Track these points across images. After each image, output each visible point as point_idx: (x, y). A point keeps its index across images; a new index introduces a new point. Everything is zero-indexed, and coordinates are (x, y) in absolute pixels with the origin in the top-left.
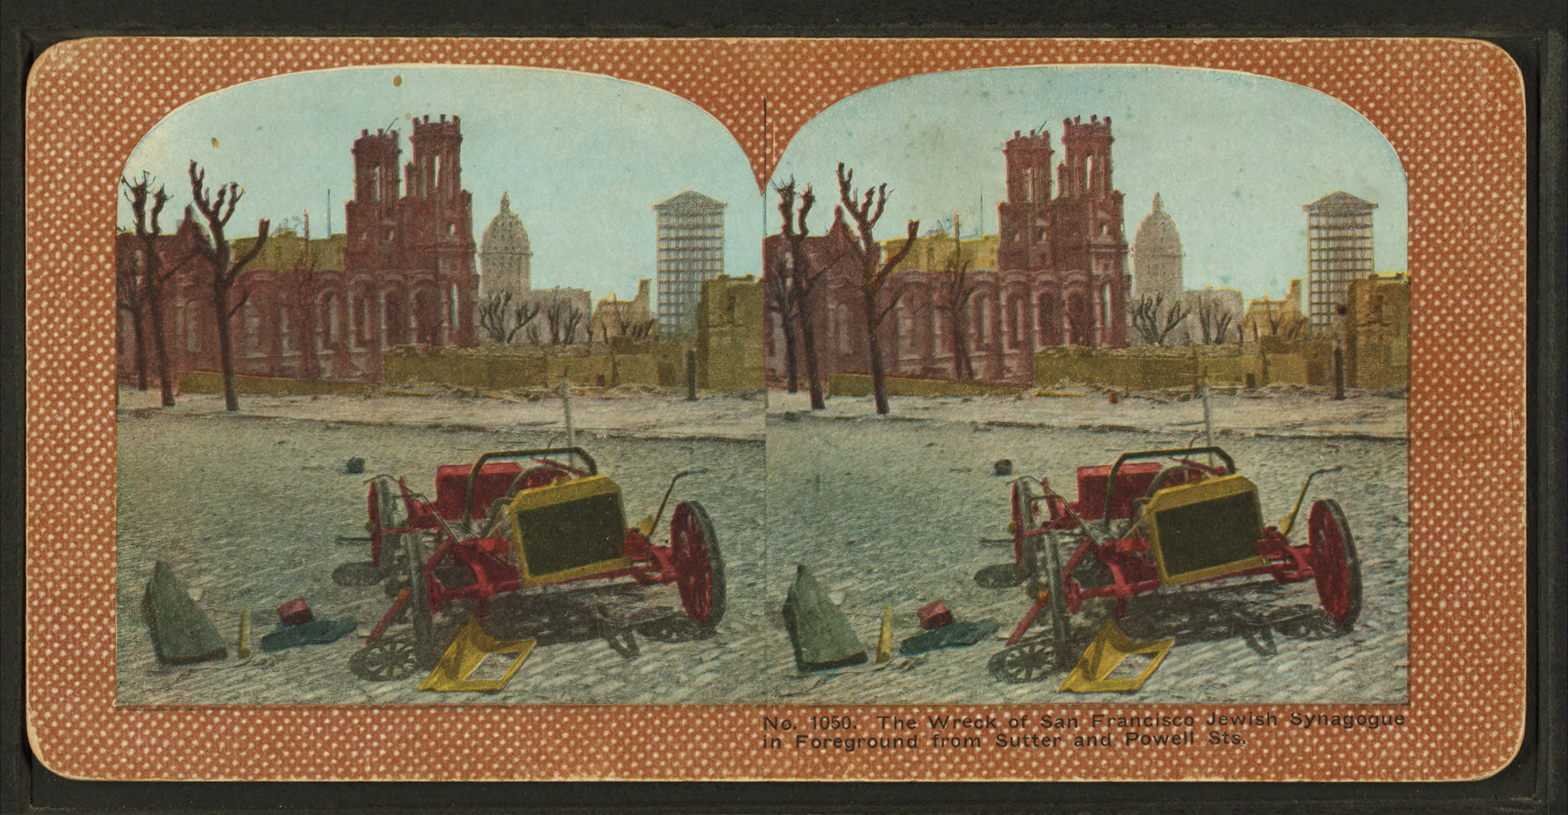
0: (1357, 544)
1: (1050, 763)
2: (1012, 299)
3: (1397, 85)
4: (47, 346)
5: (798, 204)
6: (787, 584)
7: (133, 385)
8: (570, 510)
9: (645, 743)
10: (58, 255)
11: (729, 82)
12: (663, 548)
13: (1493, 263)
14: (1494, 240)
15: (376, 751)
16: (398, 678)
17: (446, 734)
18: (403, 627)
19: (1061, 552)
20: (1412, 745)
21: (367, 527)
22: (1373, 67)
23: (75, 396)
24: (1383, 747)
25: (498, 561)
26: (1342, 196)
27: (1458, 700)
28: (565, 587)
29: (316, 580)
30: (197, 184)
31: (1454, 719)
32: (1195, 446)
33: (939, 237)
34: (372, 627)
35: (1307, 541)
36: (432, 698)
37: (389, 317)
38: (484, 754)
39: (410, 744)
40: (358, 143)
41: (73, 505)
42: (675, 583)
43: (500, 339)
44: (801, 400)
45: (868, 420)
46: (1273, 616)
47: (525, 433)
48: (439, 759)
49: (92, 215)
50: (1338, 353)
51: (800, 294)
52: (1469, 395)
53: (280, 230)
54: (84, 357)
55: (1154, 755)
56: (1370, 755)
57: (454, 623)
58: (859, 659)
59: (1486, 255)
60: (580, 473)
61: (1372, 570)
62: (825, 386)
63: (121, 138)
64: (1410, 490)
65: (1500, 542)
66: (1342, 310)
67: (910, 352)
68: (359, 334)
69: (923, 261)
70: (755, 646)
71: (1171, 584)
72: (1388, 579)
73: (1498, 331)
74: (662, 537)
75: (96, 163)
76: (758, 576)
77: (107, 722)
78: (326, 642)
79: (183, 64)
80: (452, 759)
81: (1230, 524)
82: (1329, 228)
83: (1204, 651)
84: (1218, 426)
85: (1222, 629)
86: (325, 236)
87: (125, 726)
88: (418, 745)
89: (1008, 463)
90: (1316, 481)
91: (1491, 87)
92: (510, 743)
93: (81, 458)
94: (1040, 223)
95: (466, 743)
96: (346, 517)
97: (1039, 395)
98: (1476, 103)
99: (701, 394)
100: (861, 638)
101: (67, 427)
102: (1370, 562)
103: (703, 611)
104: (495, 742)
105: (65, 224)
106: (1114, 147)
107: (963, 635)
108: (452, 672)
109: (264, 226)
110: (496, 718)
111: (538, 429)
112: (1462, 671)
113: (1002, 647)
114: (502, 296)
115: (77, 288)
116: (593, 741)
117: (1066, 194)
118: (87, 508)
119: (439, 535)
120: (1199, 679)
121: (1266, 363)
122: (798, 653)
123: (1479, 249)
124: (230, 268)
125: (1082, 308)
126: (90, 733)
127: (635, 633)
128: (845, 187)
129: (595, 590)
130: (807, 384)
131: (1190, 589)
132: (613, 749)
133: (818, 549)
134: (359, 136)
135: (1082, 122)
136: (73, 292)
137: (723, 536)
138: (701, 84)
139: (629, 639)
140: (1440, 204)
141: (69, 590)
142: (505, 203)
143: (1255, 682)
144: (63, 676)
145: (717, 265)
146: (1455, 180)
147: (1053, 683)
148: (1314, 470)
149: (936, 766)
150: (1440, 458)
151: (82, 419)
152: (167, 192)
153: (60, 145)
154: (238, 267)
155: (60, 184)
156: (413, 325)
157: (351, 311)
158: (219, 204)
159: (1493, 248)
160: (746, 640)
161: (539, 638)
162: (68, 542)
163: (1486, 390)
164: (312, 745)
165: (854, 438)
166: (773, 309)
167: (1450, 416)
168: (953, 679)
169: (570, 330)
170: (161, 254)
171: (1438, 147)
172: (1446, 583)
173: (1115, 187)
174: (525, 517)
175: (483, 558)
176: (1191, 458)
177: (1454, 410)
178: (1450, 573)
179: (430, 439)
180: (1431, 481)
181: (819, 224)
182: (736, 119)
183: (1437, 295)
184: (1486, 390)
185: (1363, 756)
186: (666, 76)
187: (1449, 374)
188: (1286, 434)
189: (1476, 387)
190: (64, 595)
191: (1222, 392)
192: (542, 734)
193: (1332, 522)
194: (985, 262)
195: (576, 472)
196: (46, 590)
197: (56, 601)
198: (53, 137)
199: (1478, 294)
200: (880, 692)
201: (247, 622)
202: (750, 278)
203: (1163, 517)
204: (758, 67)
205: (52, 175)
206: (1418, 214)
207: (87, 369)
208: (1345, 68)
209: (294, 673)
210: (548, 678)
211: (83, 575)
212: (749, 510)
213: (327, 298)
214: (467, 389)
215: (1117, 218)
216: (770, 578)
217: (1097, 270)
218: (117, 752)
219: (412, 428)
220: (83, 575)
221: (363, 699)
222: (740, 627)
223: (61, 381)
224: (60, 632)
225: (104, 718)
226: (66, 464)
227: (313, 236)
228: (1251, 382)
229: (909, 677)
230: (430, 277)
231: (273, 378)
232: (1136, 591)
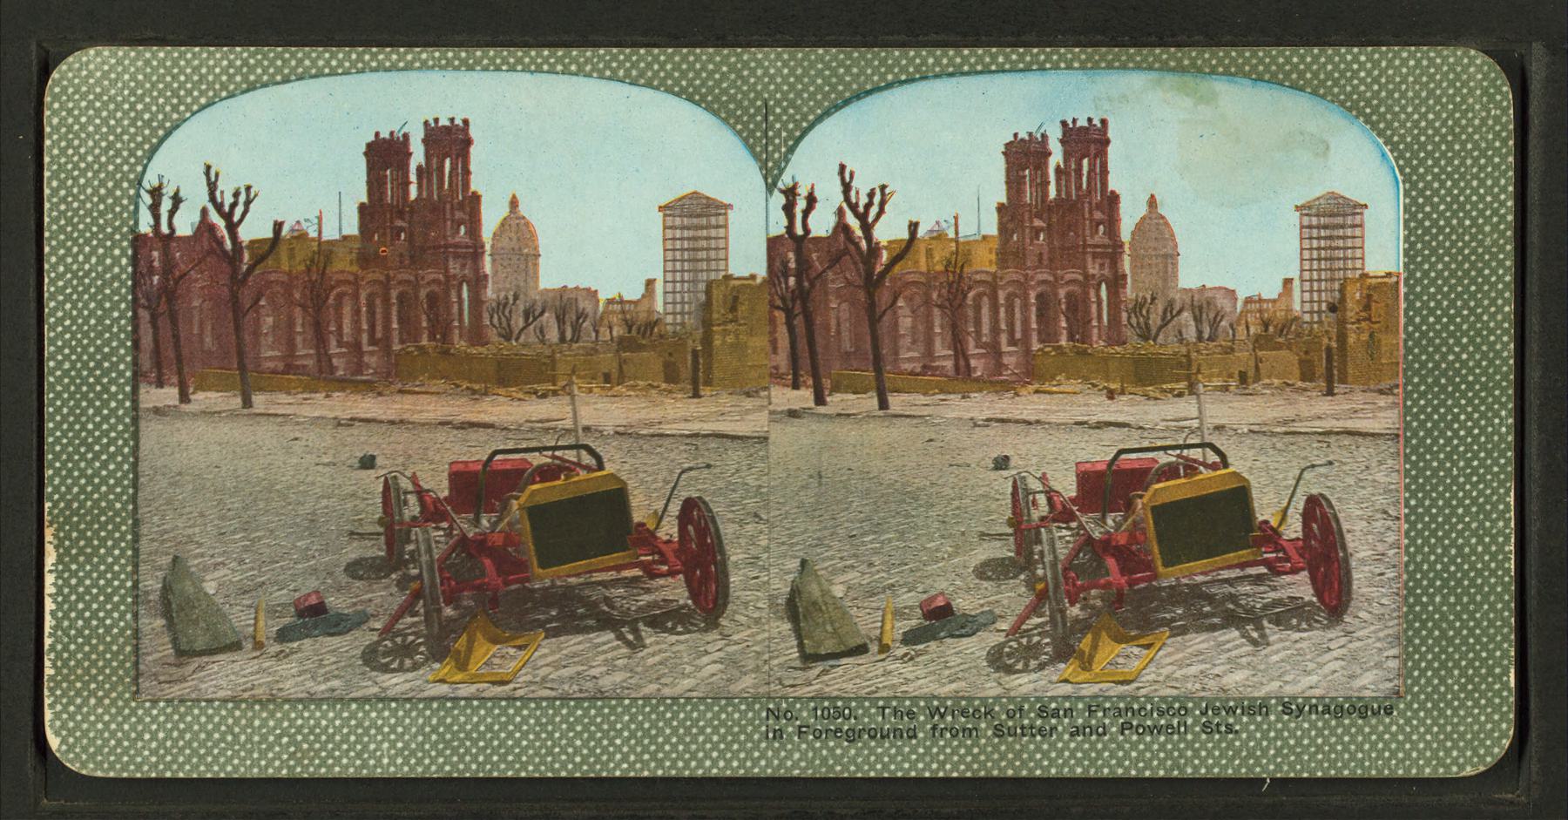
0: (1348, 537)
1: (1053, 755)
2: (1010, 298)
4: (70, 347)
5: (801, 204)
6: (790, 578)
7: (150, 383)
8: (1201, 503)
9: (657, 736)
10: (81, 258)
11: (739, 89)
12: (669, 542)
13: (1487, 264)
14: (1488, 242)
15: (393, 744)
16: (1034, 671)
17: (462, 728)
18: (1040, 620)
19: (1058, 545)
20: (1408, 738)
21: (380, 522)
22: (1369, 73)
23: (99, 396)
24: (1380, 738)
25: (522, 553)
26: (695, 196)
27: (1453, 692)
28: (573, 580)
29: (330, 574)
30: (212, 187)
31: (1449, 712)
32: (1189, 441)
33: (939, 236)
35: (1300, 535)
36: (443, 689)
37: (1040, 316)
38: (500, 746)
39: (427, 736)
40: (369, 145)
41: (96, 502)
42: (681, 576)
43: (508, 338)
44: (803, 397)
45: (870, 417)
46: (1265, 607)
47: (532, 430)
48: (455, 751)
49: (115, 218)
50: (1329, 349)
51: (802, 295)
52: (1464, 395)
53: (292, 230)
54: (106, 357)
55: (1156, 747)
56: (1367, 746)
57: (464, 616)
58: (861, 650)
60: (588, 468)
61: (1363, 561)
62: (827, 383)
63: (143, 143)
64: (1407, 487)
65: (1494, 538)
66: (1332, 308)
67: (909, 349)
68: (1011, 332)
69: (923, 260)
70: (759, 638)
71: (1167, 576)
72: (1378, 571)
73: (1491, 332)
74: (669, 530)
75: (118, 168)
76: (764, 568)
77: (130, 716)
78: (339, 634)
80: (468, 751)
81: (1222, 519)
82: (683, 228)
83: (1198, 641)
84: (1210, 422)
85: (1216, 620)
86: (337, 237)
87: (148, 719)
88: (434, 737)
89: (1007, 458)
90: (1306, 475)
91: (1485, 92)
92: (525, 735)
93: (104, 457)
94: (1038, 223)
95: (482, 736)
96: (989, 513)
97: (1037, 392)
98: (1471, 108)
99: (705, 391)
100: (863, 630)
101: (90, 426)
102: (1361, 555)
103: (710, 600)
104: (510, 735)
105: (88, 228)
107: (337, 625)
108: (1086, 663)
109: (278, 226)
110: (511, 711)
112: (1457, 665)
113: (1001, 638)
115: (100, 290)
117: (425, 194)
118: (110, 506)
119: (451, 528)
120: (1193, 670)
121: (1258, 360)
122: (801, 646)
124: (879, 269)
125: (1077, 309)
126: (113, 726)
127: (641, 626)
128: (847, 188)
129: (602, 583)
130: (810, 382)
131: (1185, 581)
133: (820, 542)
134: (372, 138)
136: (96, 294)
137: (727, 530)
138: (710, 90)
139: (635, 631)
140: (1435, 207)
141: (93, 586)
142: (514, 203)
143: (1247, 673)
145: (722, 265)
146: (1449, 183)
147: (1052, 673)
148: (1304, 464)
149: (942, 757)
150: (1435, 455)
151: (106, 419)
152: (182, 194)
153: (82, 150)
154: (251, 268)
155: (83, 189)
156: (424, 324)
157: (1002, 310)
158: (234, 205)
159: (1487, 250)
160: (749, 632)
161: (547, 631)
162: (91, 539)
163: (1481, 390)
164: (331, 738)
165: (857, 435)
166: (778, 308)
167: (1445, 414)
169: (576, 329)
170: (814, 256)
171: (1433, 151)
173: (473, 188)
175: (491, 552)
176: (1185, 452)
177: (1449, 409)
179: (441, 435)
180: (1427, 479)
181: (821, 224)
182: (746, 125)
183: (1432, 297)
184: (1481, 390)
185: (1360, 748)
186: (677, 82)
187: (1444, 373)
188: (644, 432)
189: (1470, 386)
192: (556, 727)
193: (1324, 515)
194: (984, 262)
195: (1206, 466)
196: (69, 586)
197: (80, 598)
198: (76, 142)
199: (1473, 296)
200: (881, 682)
201: (889, 616)
202: (753, 277)
205: (75, 179)
206: (1413, 216)
207: (109, 370)
208: (1343, 73)
209: (309, 665)
210: (1181, 667)
212: (751, 503)
213: (340, 297)
214: (476, 387)
215: (1112, 222)
216: (773, 570)
217: (454, 267)
218: (140, 744)
219: (423, 425)
222: (742, 619)
223: (85, 381)
225: (127, 711)
226: (90, 463)
229: (910, 667)
230: (1080, 278)
231: (289, 375)
232: (1131, 584)
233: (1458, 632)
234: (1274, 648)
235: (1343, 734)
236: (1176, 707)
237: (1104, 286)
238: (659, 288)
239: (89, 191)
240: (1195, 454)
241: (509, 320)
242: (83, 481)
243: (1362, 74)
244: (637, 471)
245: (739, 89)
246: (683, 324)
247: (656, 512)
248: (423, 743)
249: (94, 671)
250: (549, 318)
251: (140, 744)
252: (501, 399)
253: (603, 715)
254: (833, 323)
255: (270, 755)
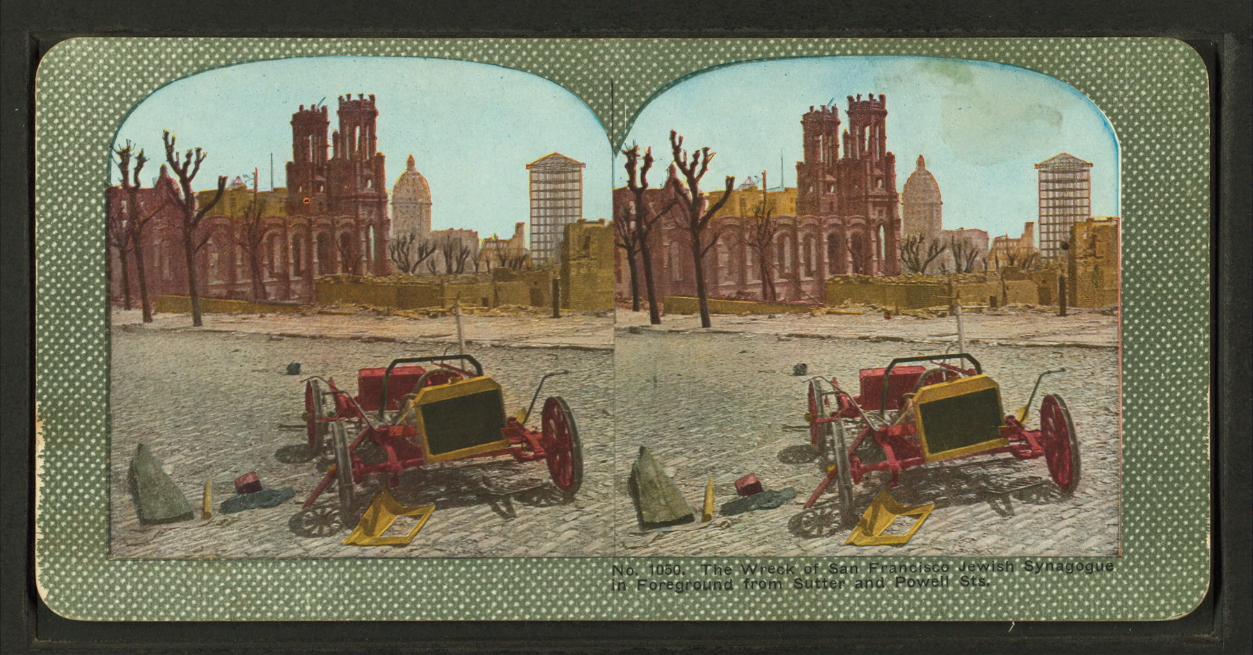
0: (1077, 429)
1: (842, 603)
2: (807, 238)
3: (1113, 73)
4: (56, 277)
5: (640, 163)
6: (631, 461)
7: (120, 306)
8: (961, 402)
9: (525, 588)
10: (65, 206)
12: (534, 433)
14: (1189, 193)
15: (314, 595)
16: (826, 536)
17: (369, 581)
19: (846, 435)
20: (1125, 590)
21: (304, 417)
22: (1094, 58)
23: (79, 316)
25: (417, 441)
26: (555, 156)
27: (1161, 553)
28: (458, 463)
29: (264, 458)
30: (170, 149)
31: (1158, 569)
32: (951, 353)
33: (750, 189)
34: (808, 495)
35: (1039, 427)
36: (354, 550)
38: (399, 596)
39: (341, 588)
40: (295, 116)
41: (77, 401)
42: (544, 460)
43: (406, 270)
44: (642, 317)
45: (695, 333)
46: (1011, 485)
47: (425, 343)
48: (363, 600)
49: (92, 175)
50: (1062, 279)
51: (641, 236)
52: (1170, 315)
53: (234, 184)
54: (85, 285)
55: (924, 596)
57: (370, 492)
58: (688, 519)
59: (1183, 205)
60: (470, 374)
61: (1089, 449)
62: (661, 306)
64: (1124, 389)
65: (1194, 430)
67: (726, 279)
68: (808, 265)
69: (737, 208)
70: (607, 509)
71: (933, 460)
72: (1101, 456)
75: (94, 134)
76: (610, 454)
78: (271, 506)
79: (163, 56)
80: (374, 600)
81: (977, 415)
82: (546, 182)
83: (958, 512)
84: (967, 337)
86: (269, 189)
87: (118, 575)
89: (804, 366)
91: (1187, 73)
92: (419, 587)
93: (83, 365)
94: (829, 178)
95: (385, 588)
96: (790, 410)
97: (828, 313)
98: (1175, 87)
99: (564, 312)
100: (690, 503)
101: (72, 340)
102: (1088, 443)
103: (567, 479)
104: (408, 587)
105: (70, 182)
106: (377, 119)
108: (868, 530)
109: (222, 181)
111: (437, 339)
112: (1164, 531)
113: (800, 510)
114: (918, 237)
115: (80, 232)
116: (484, 586)
117: (339, 155)
118: (88, 404)
119: (360, 422)
120: (954, 535)
121: (1006, 288)
122: (640, 516)
123: (1178, 201)
124: (702, 215)
125: (861, 247)
126: (90, 580)
127: (512, 500)
128: (677, 150)
130: (648, 305)
131: (947, 464)
132: (500, 592)
133: (655, 433)
134: (297, 110)
135: (862, 99)
136: (77, 235)
137: (581, 423)
138: (568, 72)
139: (508, 504)
142: (411, 162)
143: (996, 537)
144: (69, 536)
145: (577, 211)
146: (1158, 146)
150: (1147, 364)
153: (66, 120)
154: (201, 214)
155: (66, 151)
156: (339, 259)
158: (187, 164)
159: (1189, 200)
161: (437, 504)
162: (73, 431)
165: (684, 348)
166: (622, 246)
167: (1155, 331)
168: (763, 534)
169: (461, 262)
170: (651, 204)
171: (1145, 121)
172: (1152, 462)
174: (429, 410)
175: (393, 441)
176: (947, 361)
177: (1158, 327)
178: (1155, 454)
180: (1140, 383)
181: (656, 179)
183: (1144, 237)
184: (1183, 312)
185: (1087, 597)
186: (541, 66)
188: (515, 345)
189: (1175, 308)
190: (70, 472)
191: (972, 310)
192: (445, 581)
193: (1058, 411)
194: (787, 209)
195: (964, 372)
196: (55, 468)
197: (64, 478)
198: (61, 114)
199: (1177, 236)
202: (602, 221)
203: (927, 409)
204: (612, 59)
205: (60, 143)
206: (1129, 173)
207: (87, 296)
209: (247, 531)
210: (943, 533)
211: (85, 457)
212: (600, 402)
213: (272, 237)
215: (889, 177)
216: (618, 456)
217: (363, 213)
218: (112, 594)
219: (338, 339)
220: (85, 457)
221: (300, 551)
222: (593, 494)
223: (68, 305)
224: (67, 501)
225: (101, 568)
226: (72, 370)
227: (261, 189)
228: (993, 302)
229: (727, 533)
231: (231, 299)
232: (904, 466)
233: (1165, 505)
234: (1018, 517)
235: (1073, 586)
236: (940, 565)
237: (882, 228)
238: (527, 230)
239: (71, 152)
240: (955, 362)
241: (406, 256)
242: (66, 384)
243: (1089, 59)
244: (509, 376)
245: (590, 71)
246: (546, 259)
247: (524, 409)
248: (338, 594)
249: (75, 536)
250: (438, 254)
251: (112, 594)
252: (400, 319)
253: (482, 571)
254: (666, 258)
255: (216, 603)
